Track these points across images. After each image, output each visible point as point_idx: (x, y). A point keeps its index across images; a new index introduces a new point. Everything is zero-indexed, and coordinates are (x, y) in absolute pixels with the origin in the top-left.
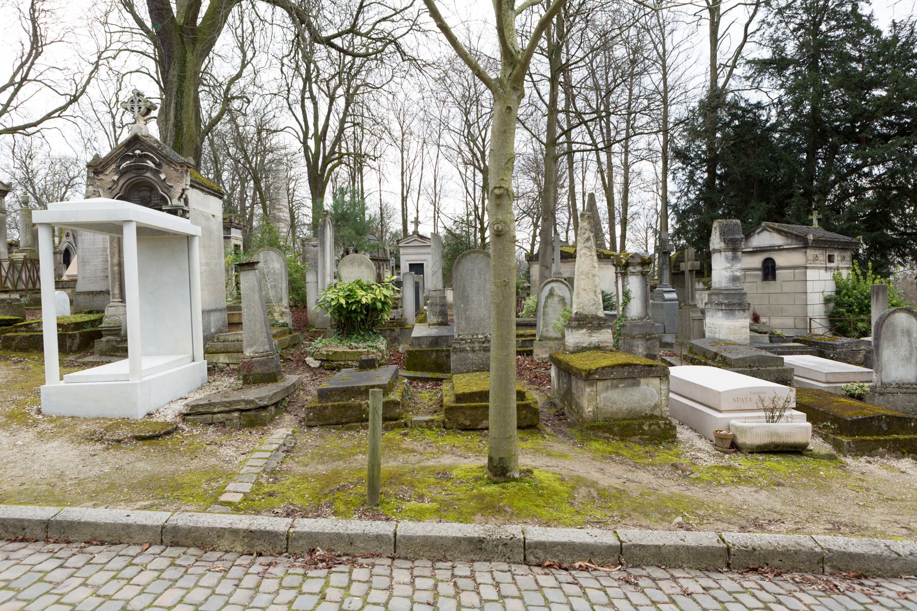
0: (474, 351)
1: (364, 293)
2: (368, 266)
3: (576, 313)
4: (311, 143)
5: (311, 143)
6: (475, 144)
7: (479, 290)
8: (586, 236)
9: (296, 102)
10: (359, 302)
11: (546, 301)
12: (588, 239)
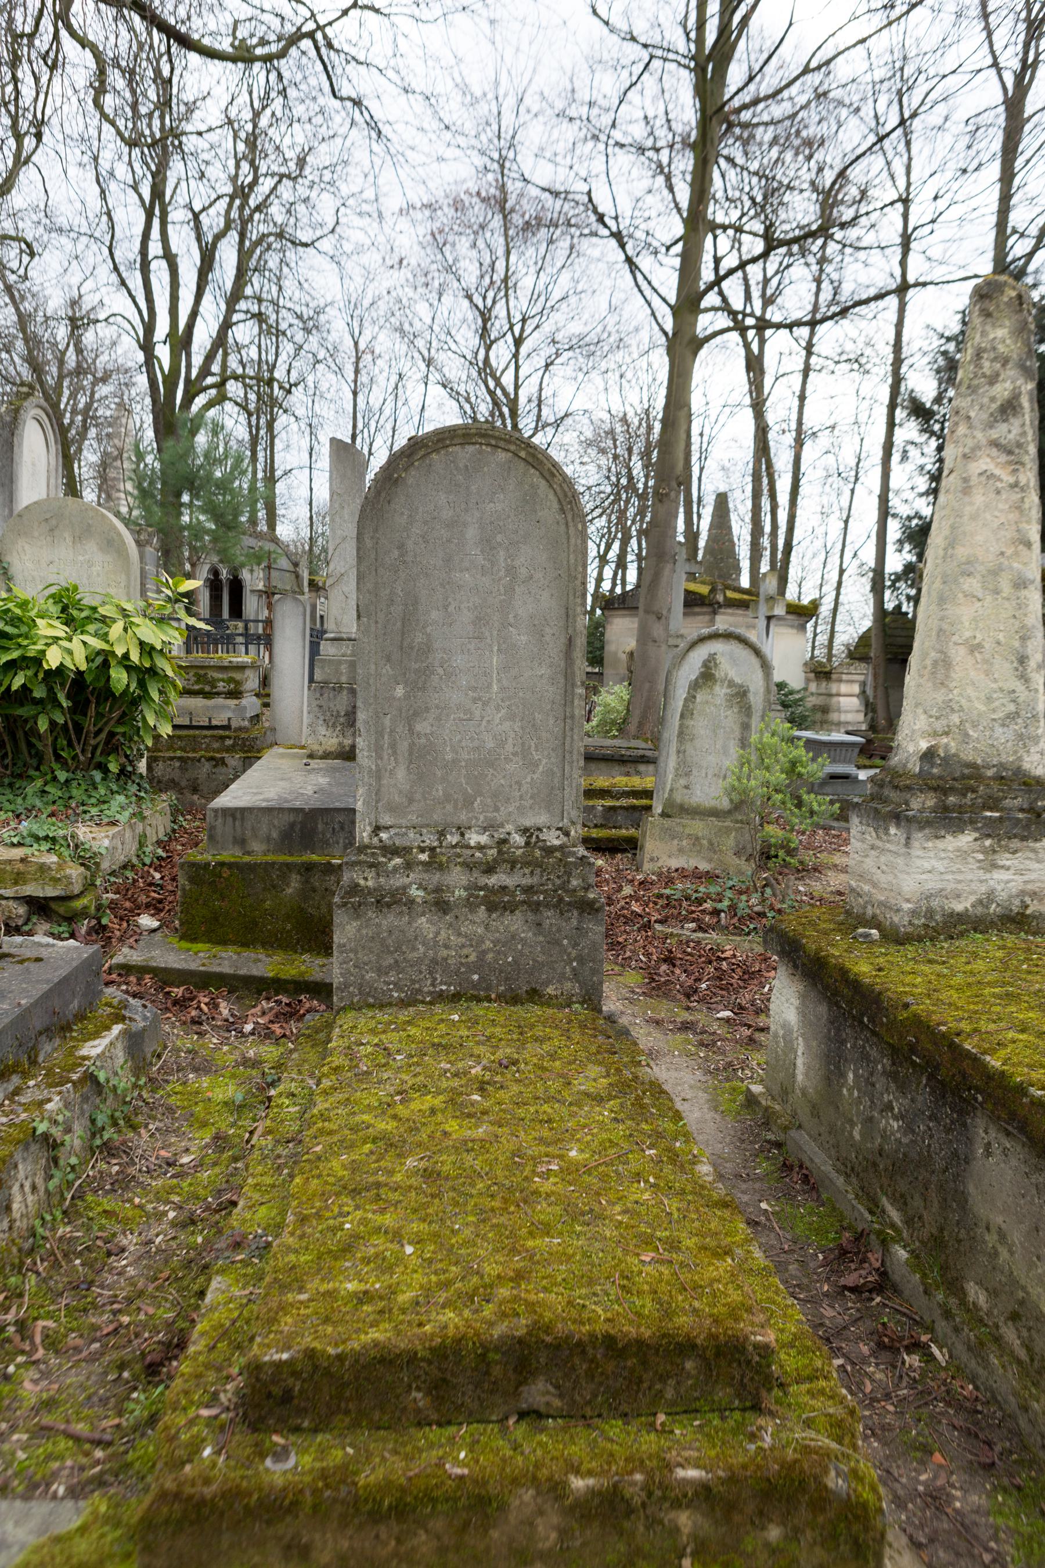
0: (441, 905)
1: (60, 630)
2: (111, 544)
3: (929, 755)
4: (163, 352)
5: (163, 352)
6: (498, 383)
7: (479, 621)
8: (1002, 390)
9: (131, 266)
10: (37, 661)
11: (691, 698)
12: (1009, 408)
